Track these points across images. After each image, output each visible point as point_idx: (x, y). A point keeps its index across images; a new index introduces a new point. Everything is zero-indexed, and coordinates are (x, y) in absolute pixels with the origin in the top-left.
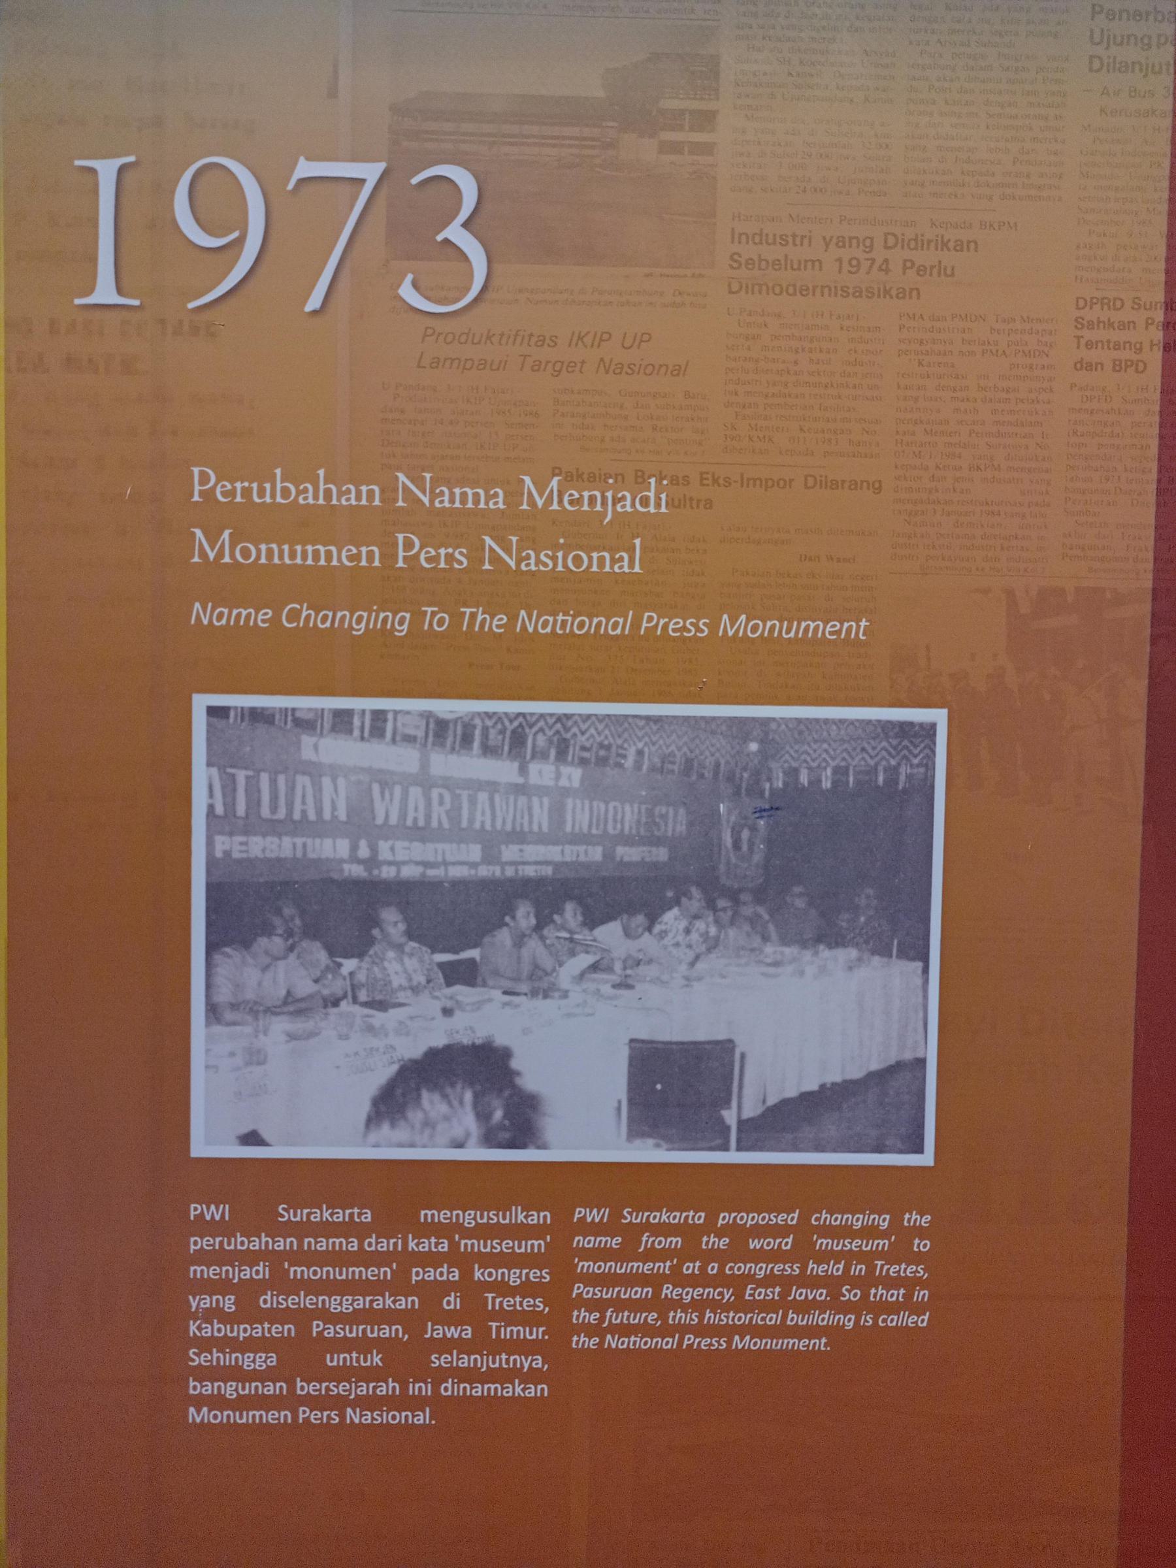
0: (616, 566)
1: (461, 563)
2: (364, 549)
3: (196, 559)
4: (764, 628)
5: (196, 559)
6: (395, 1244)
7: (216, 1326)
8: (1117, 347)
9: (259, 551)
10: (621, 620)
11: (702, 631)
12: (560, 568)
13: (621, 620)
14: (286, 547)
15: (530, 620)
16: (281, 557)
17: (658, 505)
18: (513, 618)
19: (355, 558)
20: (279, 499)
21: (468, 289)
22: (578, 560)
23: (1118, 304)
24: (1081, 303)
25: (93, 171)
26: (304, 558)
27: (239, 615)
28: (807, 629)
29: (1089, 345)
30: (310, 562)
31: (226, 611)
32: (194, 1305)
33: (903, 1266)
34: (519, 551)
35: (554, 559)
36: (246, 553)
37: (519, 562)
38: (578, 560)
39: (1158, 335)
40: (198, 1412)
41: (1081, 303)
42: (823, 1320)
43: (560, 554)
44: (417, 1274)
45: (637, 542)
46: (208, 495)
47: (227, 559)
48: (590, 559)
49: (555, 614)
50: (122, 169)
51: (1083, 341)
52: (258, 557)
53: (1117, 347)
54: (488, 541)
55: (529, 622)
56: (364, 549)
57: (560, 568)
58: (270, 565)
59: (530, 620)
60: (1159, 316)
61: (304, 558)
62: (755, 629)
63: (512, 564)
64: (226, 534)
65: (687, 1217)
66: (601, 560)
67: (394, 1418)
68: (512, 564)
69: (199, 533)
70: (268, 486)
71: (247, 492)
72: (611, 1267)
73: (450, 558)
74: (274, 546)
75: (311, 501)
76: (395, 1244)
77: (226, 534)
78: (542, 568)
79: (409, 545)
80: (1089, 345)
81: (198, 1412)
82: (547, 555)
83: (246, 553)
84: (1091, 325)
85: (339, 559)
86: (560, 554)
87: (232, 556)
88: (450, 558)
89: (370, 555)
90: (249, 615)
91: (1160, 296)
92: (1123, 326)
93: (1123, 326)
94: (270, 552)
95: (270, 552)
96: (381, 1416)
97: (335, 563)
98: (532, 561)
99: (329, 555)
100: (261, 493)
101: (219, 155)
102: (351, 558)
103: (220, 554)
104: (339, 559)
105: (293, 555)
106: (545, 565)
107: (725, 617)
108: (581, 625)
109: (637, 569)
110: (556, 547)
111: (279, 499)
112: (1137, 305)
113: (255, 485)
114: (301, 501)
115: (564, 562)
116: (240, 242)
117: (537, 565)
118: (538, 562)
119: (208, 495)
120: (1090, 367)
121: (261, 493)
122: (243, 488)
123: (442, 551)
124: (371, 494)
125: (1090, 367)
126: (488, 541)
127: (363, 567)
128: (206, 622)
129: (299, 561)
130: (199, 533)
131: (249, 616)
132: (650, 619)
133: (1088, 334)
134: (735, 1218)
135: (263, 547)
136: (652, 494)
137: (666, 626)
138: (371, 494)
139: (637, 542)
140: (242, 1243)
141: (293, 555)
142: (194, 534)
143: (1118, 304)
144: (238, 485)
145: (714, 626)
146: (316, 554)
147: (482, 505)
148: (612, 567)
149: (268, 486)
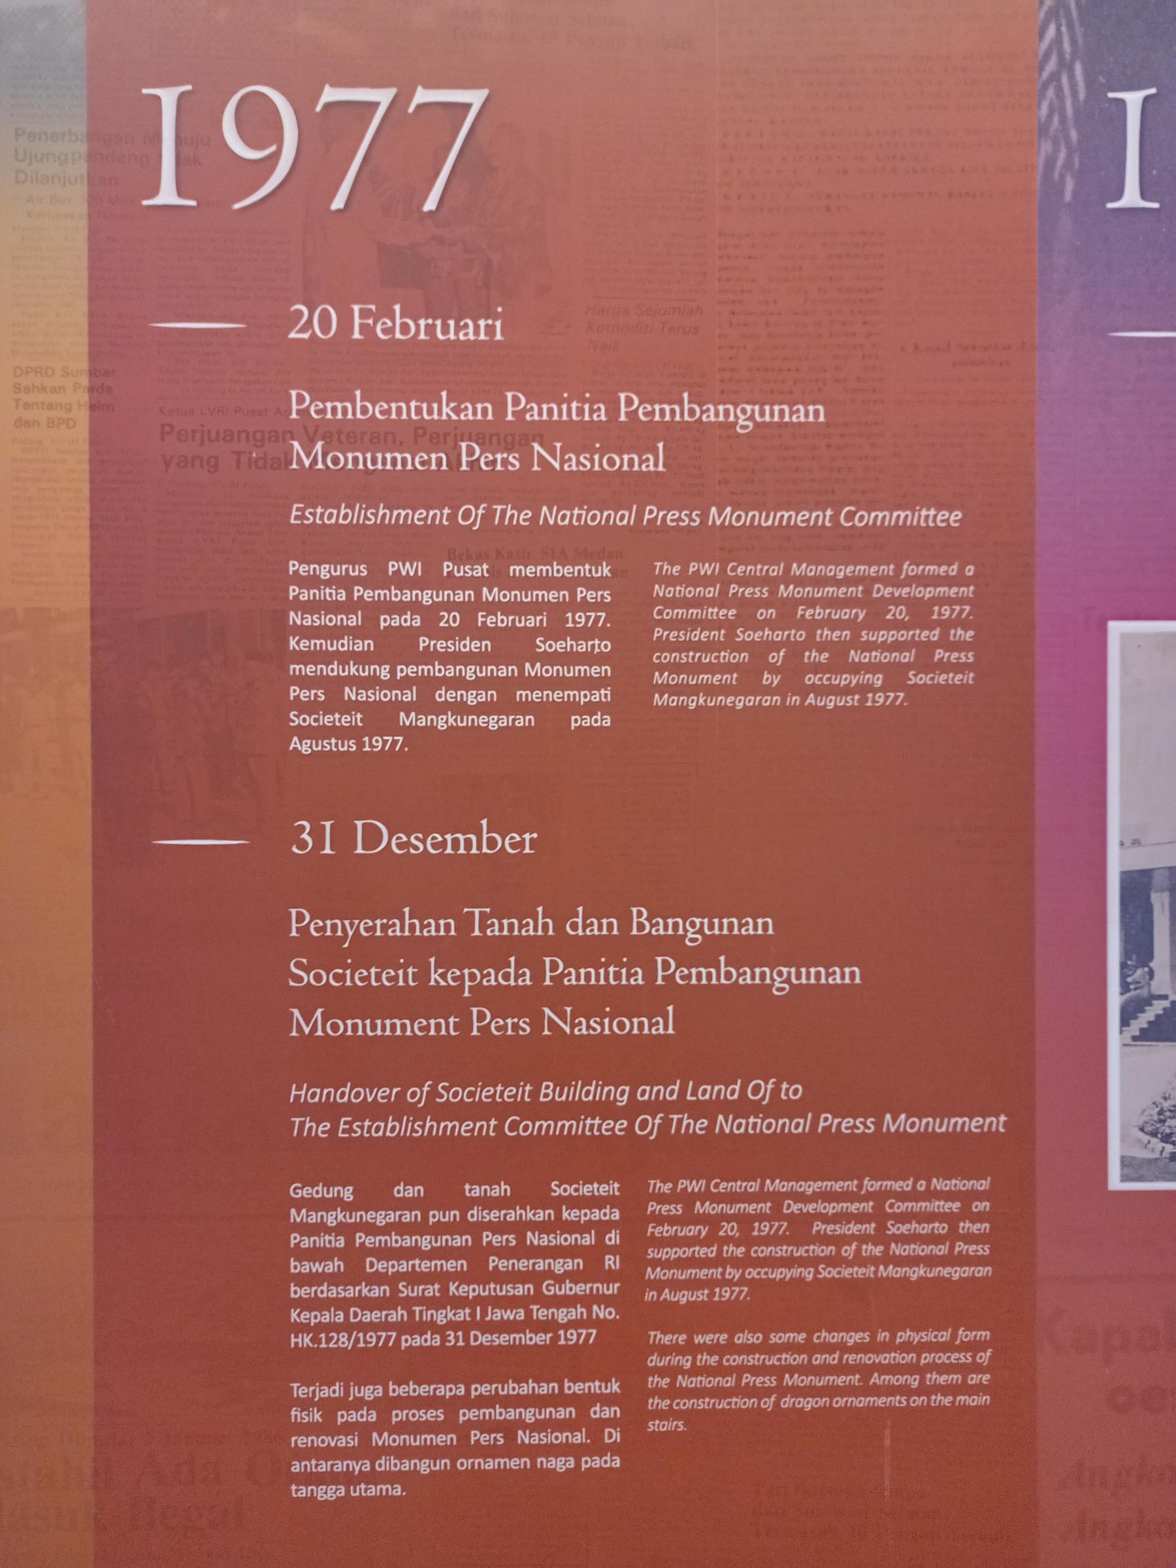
0: (653, 1029)
1: (524, 1030)
3: (294, 1034)
5: (294, 1034)
6: (541, 621)
7: (394, 1238)
8: (50, 407)
10: (802, 1121)
11: (869, 1128)
14: (368, 1022)
15: (727, 1122)
16: (598, 979)
19: (387, 412)
20: (723, 981)
22: (621, 1026)
23: (50, 371)
24: (19, 372)
27: (446, 1127)
28: (956, 1124)
29: (27, 406)
31: (318, 1091)
33: (367, 1123)
34: (562, 456)
36: (335, 1027)
38: (621, 1026)
39: (85, 397)
40: (380, 1436)
41: (19, 372)
44: (402, 671)
45: (670, 1008)
48: (632, 1024)
51: (21, 404)
52: (346, 1030)
53: (50, 407)
58: (355, 1037)
59: (727, 1122)
60: (85, 381)
61: (384, 463)
62: (913, 1125)
64: (319, 1012)
65: (789, 635)
66: (641, 1025)
67: (386, 696)
69: (296, 1012)
73: (516, 1027)
74: (408, 1022)
76: (541, 621)
77: (319, 1012)
78: (592, 1032)
80: (27, 406)
81: (380, 1436)
82: (596, 1022)
83: (335, 1027)
84: (27, 390)
85: (412, 1030)
86: (606, 1021)
87: (324, 1030)
88: (505, 462)
90: (454, 1127)
91: (84, 365)
92: (54, 390)
93: (54, 390)
94: (355, 1027)
95: (355, 1027)
96: (374, 694)
97: (408, 1033)
98: (584, 1027)
99: (404, 1027)
102: (420, 1029)
104: (413, 464)
105: (374, 1028)
106: (595, 1030)
109: (671, 1031)
110: (593, 451)
111: (485, 850)
112: (66, 373)
114: (654, 933)
117: (577, 465)
120: (28, 424)
122: (513, 1024)
123: (509, 1021)
125: (28, 424)
126: (547, 1011)
127: (433, 1036)
129: (379, 1032)
130: (296, 1012)
131: (454, 1127)
132: (826, 1119)
133: (25, 398)
139: (670, 1008)
140: (396, 595)
141: (374, 1028)
142: (292, 1013)
143: (50, 371)
144: (509, 1021)
145: (879, 1124)
148: (520, 931)
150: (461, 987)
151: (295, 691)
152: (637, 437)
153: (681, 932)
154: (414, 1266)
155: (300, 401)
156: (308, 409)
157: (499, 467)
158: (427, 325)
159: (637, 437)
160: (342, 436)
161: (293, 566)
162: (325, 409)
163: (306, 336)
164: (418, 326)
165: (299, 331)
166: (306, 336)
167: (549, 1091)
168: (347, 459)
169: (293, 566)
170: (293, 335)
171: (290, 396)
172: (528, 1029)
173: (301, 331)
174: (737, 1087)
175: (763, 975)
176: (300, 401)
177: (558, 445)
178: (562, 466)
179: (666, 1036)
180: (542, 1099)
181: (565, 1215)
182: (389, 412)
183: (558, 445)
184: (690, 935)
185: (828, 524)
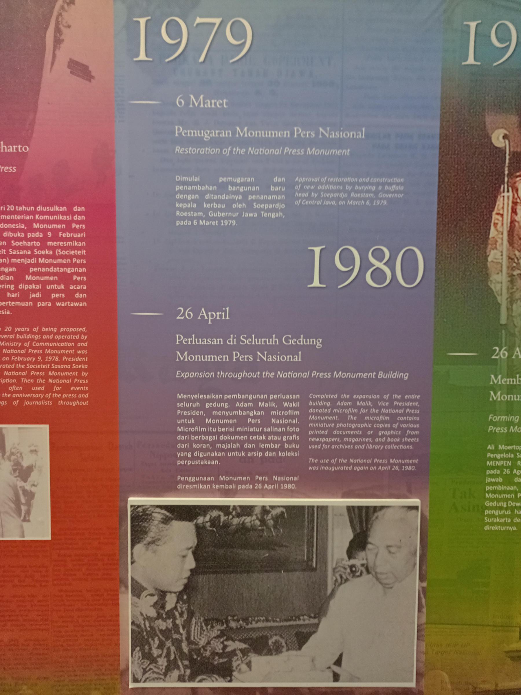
2: (224, 356)
4: (346, 375)
9: (195, 358)
12: (278, 360)
13: (306, 374)
17: (233, 342)
18: (276, 374)
19: (222, 359)
21: (414, 282)
22: (283, 358)
25: (313, 251)
26: (208, 359)
30: (209, 360)
32: (179, 455)
34: (267, 356)
35: (277, 358)
36: (191, 358)
37: (267, 359)
38: (283, 358)
42: (394, 376)
43: (278, 357)
46: (181, 342)
47: (186, 360)
49: (288, 372)
50: (321, 250)
54: (259, 353)
55: (280, 374)
56: (224, 356)
57: (278, 360)
61: (208, 359)
63: (265, 359)
64: (186, 353)
66: (290, 358)
68: (265, 359)
69: (178, 353)
70: (271, 340)
71: (265, 342)
72: (300, 375)
73: (248, 358)
75: (215, 343)
77: (186, 353)
79: (236, 355)
83: (191, 358)
86: (278, 357)
87: (188, 359)
88: (248, 358)
89: (226, 358)
94: (198, 358)
95: (198, 358)
99: (214, 358)
100: (269, 342)
101: (378, 245)
102: (220, 359)
103: (184, 358)
105: (204, 358)
107: (335, 372)
108: (207, 375)
110: (277, 355)
113: (267, 340)
115: (279, 359)
116: (352, 270)
118: (272, 358)
119: (181, 342)
121: (269, 342)
123: (246, 356)
124: (220, 341)
126: (259, 353)
128: (281, 377)
129: (206, 360)
130: (178, 353)
132: (314, 373)
134: (227, 375)
135: (196, 356)
136: (232, 339)
137: (319, 375)
138: (220, 341)
139: (300, 353)
141: (204, 358)
144: (246, 356)
145: (332, 375)
146: (211, 358)
147: (292, 360)
149: (271, 340)
150: (204, 99)
151: (314, 373)
152: (293, 350)
153: (315, 343)
154: (67, 304)
155: (179, 338)
156: (181, 133)
157: (246, 360)
158: (220, 315)
159: (293, 350)
160: (193, 350)
161: (179, 477)
162: (306, 134)
163: (183, 318)
164: (216, 315)
165: (180, 316)
166: (183, 318)
167: (382, 375)
168: (195, 358)
169: (85, 304)
170: (178, 318)
171: (176, 337)
172: (252, 359)
173: (181, 316)
174: (313, 375)
175: (313, 341)
176: (179, 338)
177: (266, 353)
178: (267, 359)
179: (298, 362)
180: (518, 417)
181: (280, 454)
182: (222, 358)
183: (266, 353)
184: (318, 345)
185: (374, 377)
